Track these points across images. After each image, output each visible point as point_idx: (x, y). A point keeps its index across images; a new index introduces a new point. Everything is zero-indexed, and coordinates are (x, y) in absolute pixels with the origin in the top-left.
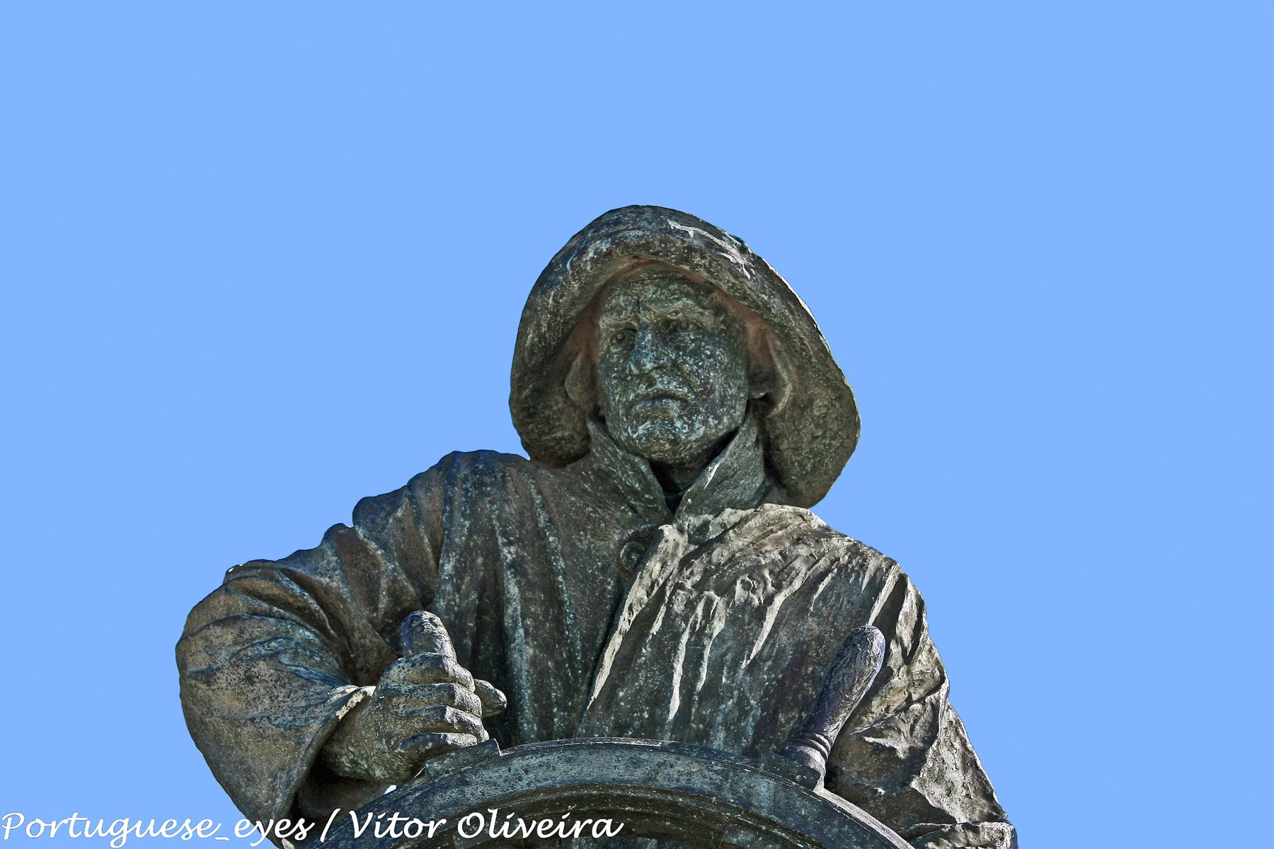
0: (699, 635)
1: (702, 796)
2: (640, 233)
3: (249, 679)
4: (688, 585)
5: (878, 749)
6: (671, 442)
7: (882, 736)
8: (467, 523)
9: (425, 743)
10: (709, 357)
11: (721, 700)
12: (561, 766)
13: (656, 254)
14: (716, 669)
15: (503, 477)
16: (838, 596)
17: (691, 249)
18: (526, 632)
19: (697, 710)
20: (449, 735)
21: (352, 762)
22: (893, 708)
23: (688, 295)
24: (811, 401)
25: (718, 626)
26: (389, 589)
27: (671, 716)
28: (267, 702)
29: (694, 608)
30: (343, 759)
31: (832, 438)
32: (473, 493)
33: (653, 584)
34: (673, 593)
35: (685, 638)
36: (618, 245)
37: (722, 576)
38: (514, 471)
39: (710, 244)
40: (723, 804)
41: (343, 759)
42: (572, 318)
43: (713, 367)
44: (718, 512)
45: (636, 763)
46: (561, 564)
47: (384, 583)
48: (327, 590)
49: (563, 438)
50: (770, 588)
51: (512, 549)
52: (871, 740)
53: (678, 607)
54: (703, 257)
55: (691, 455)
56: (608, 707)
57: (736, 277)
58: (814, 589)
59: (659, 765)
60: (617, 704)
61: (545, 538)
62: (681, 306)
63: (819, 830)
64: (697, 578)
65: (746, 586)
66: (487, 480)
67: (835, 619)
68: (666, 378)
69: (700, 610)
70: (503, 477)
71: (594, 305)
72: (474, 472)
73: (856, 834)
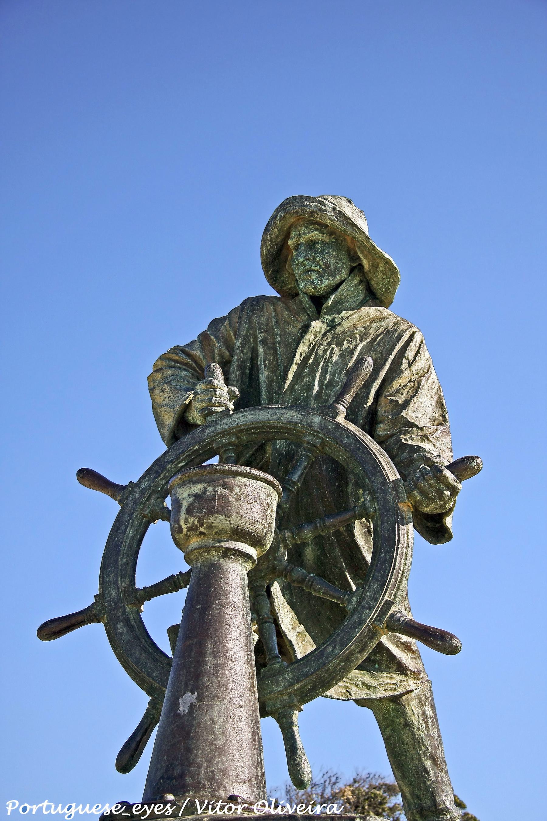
0: (327, 362)
1: (296, 424)
2: (294, 207)
3: (163, 391)
4: (325, 343)
5: (392, 401)
6: (313, 288)
7: (395, 396)
8: (247, 326)
9: (205, 411)
10: (327, 253)
11: (334, 387)
12: (249, 417)
13: (301, 215)
14: (333, 375)
15: (263, 306)
16: (384, 343)
17: (313, 212)
18: (265, 366)
19: (325, 391)
20: (214, 408)
21: (193, 419)
22: (402, 385)
23: (317, 230)
24: (378, 265)
25: (335, 358)
26: (218, 354)
27: (314, 393)
28: (167, 399)
29: (326, 352)
30: (190, 418)
31: (390, 278)
32: (250, 313)
33: (310, 344)
34: (318, 347)
35: (322, 364)
36: (287, 213)
37: (339, 339)
38: (267, 303)
39: (320, 209)
40: (303, 426)
41: (190, 418)
42: (279, 242)
43: (329, 257)
44: (339, 313)
45: (274, 414)
46: (279, 339)
47: (216, 351)
48: (196, 356)
49: (291, 288)
50: (358, 341)
51: (262, 335)
52: (389, 398)
53: (320, 352)
54: (318, 215)
55: (326, 292)
56: (291, 393)
57: (332, 221)
58: (375, 340)
59: (282, 414)
60: (295, 391)
61: (274, 329)
62: (315, 235)
63: (334, 433)
64: (329, 340)
65: (348, 342)
66: (256, 308)
67: (382, 351)
68: (310, 263)
69: (328, 353)
70: (263, 306)
71: (287, 236)
72: (252, 306)
73: (347, 434)
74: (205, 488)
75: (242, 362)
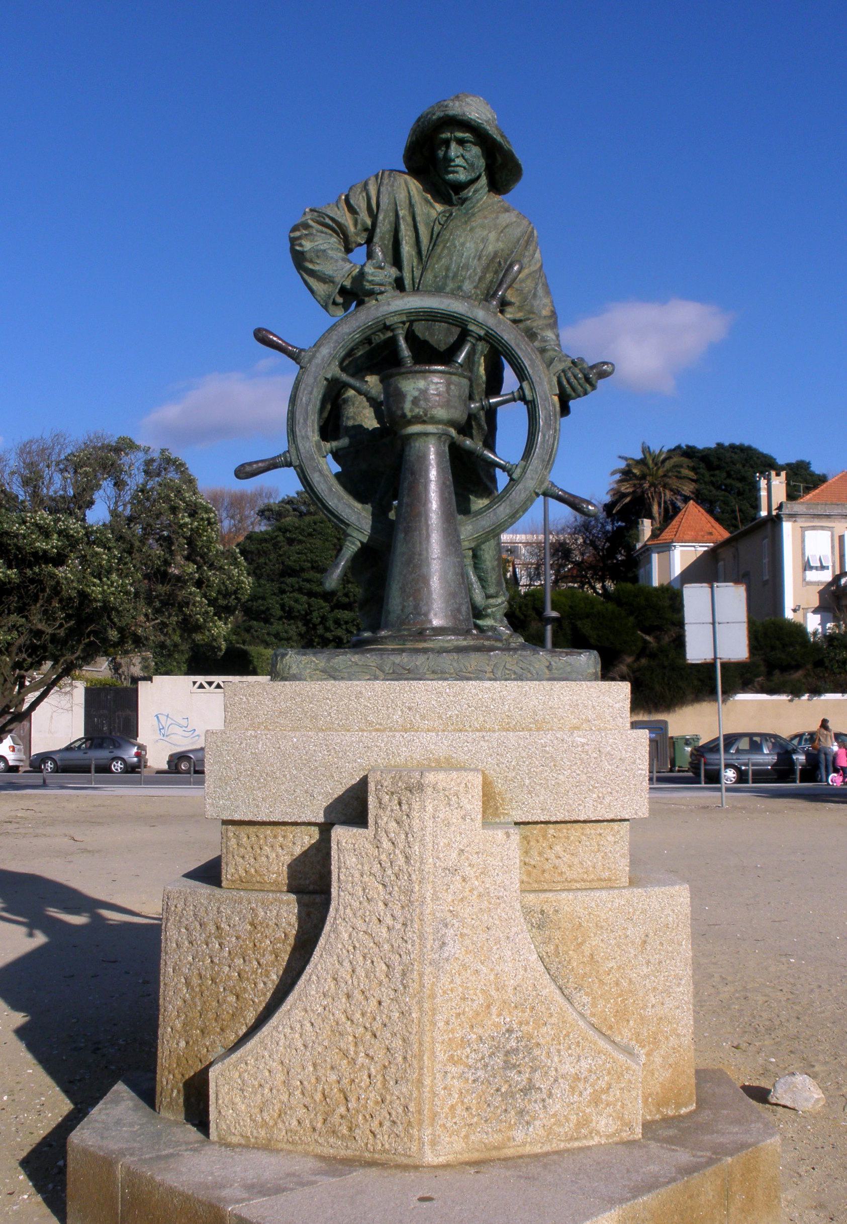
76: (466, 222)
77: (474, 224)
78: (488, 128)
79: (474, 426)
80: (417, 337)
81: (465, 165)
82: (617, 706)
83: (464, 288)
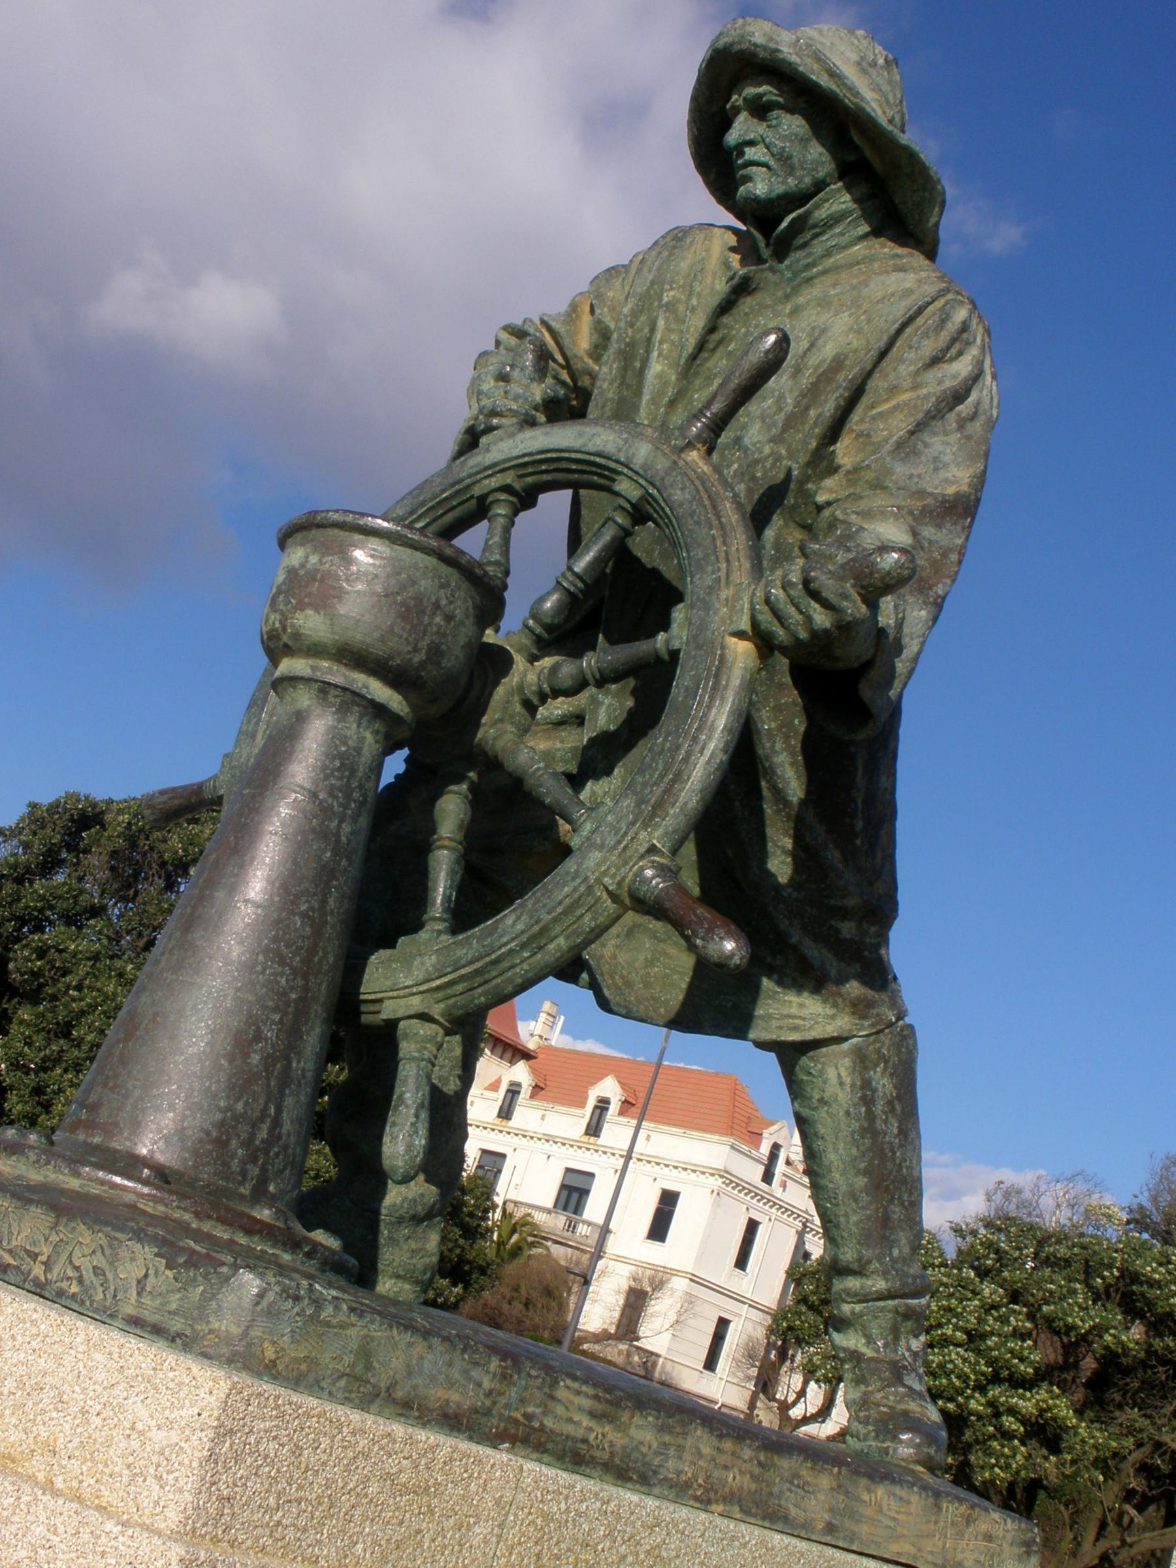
18: (660, 355)
74: (307, 557)
75: (627, 345)
76: (787, 297)
77: (801, 300)
78: (794, 59)
79: (766, 792)
80: (637, 560)
81: (767, 158)
82: (158, 1436)
83: (747, 441)
